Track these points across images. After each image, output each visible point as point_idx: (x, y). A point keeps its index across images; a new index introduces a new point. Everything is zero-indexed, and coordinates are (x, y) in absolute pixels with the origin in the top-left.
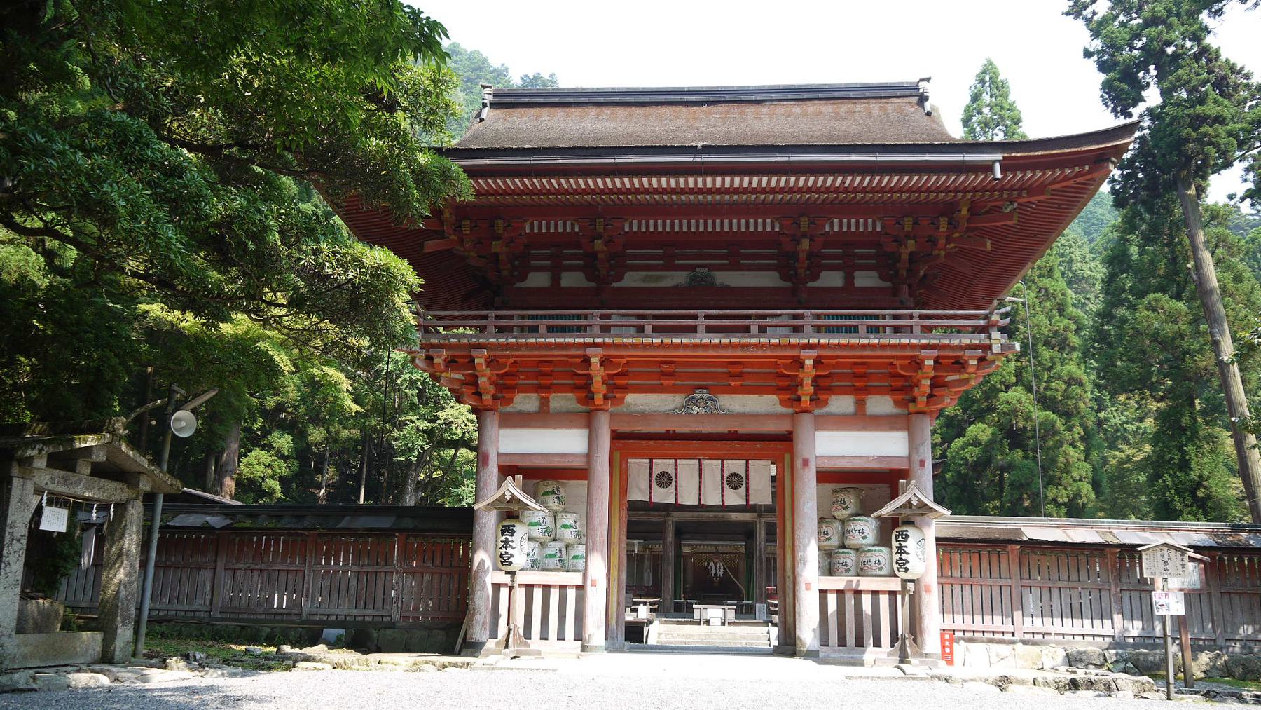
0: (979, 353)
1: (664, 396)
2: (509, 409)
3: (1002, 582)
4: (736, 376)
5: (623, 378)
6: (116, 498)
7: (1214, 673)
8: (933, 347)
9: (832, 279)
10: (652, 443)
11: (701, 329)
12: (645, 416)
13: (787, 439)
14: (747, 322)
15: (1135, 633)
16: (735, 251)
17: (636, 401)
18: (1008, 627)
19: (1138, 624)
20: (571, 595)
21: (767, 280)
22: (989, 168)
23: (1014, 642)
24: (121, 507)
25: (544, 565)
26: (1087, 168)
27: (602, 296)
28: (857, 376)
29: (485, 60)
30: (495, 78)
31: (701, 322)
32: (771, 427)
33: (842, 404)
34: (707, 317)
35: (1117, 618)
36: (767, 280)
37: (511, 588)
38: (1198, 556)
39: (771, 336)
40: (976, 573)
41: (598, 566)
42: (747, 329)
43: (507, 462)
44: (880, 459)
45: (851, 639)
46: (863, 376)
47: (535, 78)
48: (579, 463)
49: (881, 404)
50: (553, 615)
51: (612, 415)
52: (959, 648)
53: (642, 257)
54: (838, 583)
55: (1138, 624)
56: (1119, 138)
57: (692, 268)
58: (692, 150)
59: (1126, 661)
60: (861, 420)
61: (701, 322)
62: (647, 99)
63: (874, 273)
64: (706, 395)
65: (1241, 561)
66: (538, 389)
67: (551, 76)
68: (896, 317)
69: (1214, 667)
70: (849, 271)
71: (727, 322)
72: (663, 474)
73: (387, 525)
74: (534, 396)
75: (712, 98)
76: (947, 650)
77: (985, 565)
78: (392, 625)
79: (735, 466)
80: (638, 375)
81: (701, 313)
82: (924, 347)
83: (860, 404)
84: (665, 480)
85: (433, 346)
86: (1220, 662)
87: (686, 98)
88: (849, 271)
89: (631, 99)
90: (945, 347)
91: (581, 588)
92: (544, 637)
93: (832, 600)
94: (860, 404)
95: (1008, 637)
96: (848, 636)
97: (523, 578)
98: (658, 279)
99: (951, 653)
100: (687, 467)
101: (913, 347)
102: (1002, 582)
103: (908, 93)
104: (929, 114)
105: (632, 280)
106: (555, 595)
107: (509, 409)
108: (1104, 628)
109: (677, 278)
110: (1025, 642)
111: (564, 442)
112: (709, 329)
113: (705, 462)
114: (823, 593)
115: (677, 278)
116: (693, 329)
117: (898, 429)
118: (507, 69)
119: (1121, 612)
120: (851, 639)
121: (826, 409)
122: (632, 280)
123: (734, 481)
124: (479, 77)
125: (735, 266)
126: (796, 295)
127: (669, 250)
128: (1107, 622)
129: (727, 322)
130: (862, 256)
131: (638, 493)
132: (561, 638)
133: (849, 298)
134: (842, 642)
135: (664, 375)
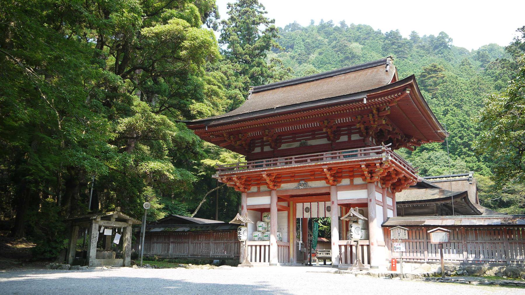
0: (379, 161)
1: (292, 184)
2: (249, 191)
3: (420, 241)
4: (315, 175)
5: (278, 179)
6: (123, 226)
7: (500, 275)
8: (364, 161)
9: (344, 138)
10: (301, 198)
11: (293, 162)
12: (287, 190)
13: (328, 194)
14: (306, 159)
15: (471, 259)
16: (314, 133)
17: (284, 186)
18: (422, 257)
19: (474, 255)
20: (365, 248)
21: (324, 141)
22: (362, 100)
23: (423, 263)
24: (125, 229)
25: (263, 240)
26: (400, 94)
27: (276, 154)
28: (350, 172)
29: (371, 29)
30: (376, 36)
31: (294, 160)
32: (323, 191)
33: (346, 182)
34: (296, 158)
35: (465, 253)
36: (324, 141)
37: (356, 247)
38: (446, 230)
39: (328, 160)
40: (456, 238)
41: (273, 240)
42: (306, 161)
43: (249, 208)
44: (358, 200)
45: (349, 261)
46: (353, 171)
47: (391, 33)
48: (268, 207)
49: (358, 181)
50: (262, 255)
51: (277, 191)
52: (398, 265)
53: (286, 139)
54: (344, 242)
55: (474, 255)
56: (407, 82)
57: (300, 141)
58: (272, 109)
59: (464, 270)
60: (352, 187)
61: (294, 160)
62: (297, 82)
63: (358, 135)
64: (303, 182)
65: (518, 230)
66: (258, 184)
67: (397, 30)
68: (365, 150)
69: (500, 272)
70: (349, 135)
71: (300, 159)
72: (307, 208)
73: (227, 228)
74: (256, 187)
75: (317, 78)
76: (394, 266)
77: (414, 234)
78: (232, 259)
79: (307, 205)
80: (284, 178)
81: (293, 157)
82: (361, 161)
83: (352, 181)
84: (308, 210)
85: (222, 175)
86: (502, 271)
87: (309, 80)
88: (349, 135)
89: (292, 83)
90: (368, 160)
91: (269, 246)
92: (256, 261)
93: (343, 248)
94: (352, 181)
95: (422, 261)
96: (348, 259)
97: (360, 243)
98: (291, 145)
99: (395, 267)
100: (314, 205)
101: (357, 161)
102: (420, 241)
103: (382, 63)
104: (387, 71)
105: (284, 147)
106: (263, 248)
107: (249, 191)
108: (462, 257)
109: (296, 145)
110: (428, 263)
111: (263, 201)
112: (296, 162)
113: (320, 203)
114: (340, 246)
115: (296, 145)
116: (291, 163)
117: (364, 189)
118: (380, 31)
119: (467, 251)
120: (349, 261)
121: (341, 184)
122: (284, 147)
123: (308, 210)
124: (369, 37)
125: (314, 138)
126: (333, 146)
127: (294, 135)
128: (461, 255)
129: (300, 159)
130: (344, 131)
131: (299, 215)
132: (265, 261)
133: (352, 145)
134: (346, 262)
135: (293, 177)
